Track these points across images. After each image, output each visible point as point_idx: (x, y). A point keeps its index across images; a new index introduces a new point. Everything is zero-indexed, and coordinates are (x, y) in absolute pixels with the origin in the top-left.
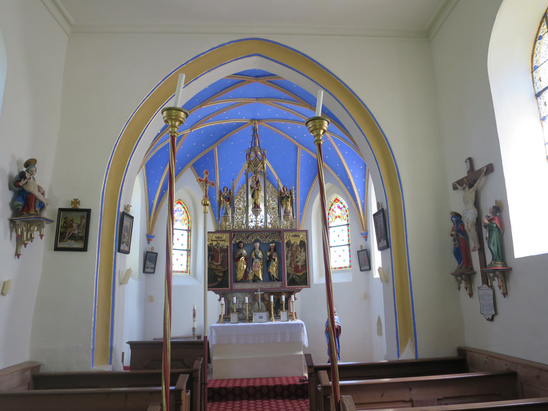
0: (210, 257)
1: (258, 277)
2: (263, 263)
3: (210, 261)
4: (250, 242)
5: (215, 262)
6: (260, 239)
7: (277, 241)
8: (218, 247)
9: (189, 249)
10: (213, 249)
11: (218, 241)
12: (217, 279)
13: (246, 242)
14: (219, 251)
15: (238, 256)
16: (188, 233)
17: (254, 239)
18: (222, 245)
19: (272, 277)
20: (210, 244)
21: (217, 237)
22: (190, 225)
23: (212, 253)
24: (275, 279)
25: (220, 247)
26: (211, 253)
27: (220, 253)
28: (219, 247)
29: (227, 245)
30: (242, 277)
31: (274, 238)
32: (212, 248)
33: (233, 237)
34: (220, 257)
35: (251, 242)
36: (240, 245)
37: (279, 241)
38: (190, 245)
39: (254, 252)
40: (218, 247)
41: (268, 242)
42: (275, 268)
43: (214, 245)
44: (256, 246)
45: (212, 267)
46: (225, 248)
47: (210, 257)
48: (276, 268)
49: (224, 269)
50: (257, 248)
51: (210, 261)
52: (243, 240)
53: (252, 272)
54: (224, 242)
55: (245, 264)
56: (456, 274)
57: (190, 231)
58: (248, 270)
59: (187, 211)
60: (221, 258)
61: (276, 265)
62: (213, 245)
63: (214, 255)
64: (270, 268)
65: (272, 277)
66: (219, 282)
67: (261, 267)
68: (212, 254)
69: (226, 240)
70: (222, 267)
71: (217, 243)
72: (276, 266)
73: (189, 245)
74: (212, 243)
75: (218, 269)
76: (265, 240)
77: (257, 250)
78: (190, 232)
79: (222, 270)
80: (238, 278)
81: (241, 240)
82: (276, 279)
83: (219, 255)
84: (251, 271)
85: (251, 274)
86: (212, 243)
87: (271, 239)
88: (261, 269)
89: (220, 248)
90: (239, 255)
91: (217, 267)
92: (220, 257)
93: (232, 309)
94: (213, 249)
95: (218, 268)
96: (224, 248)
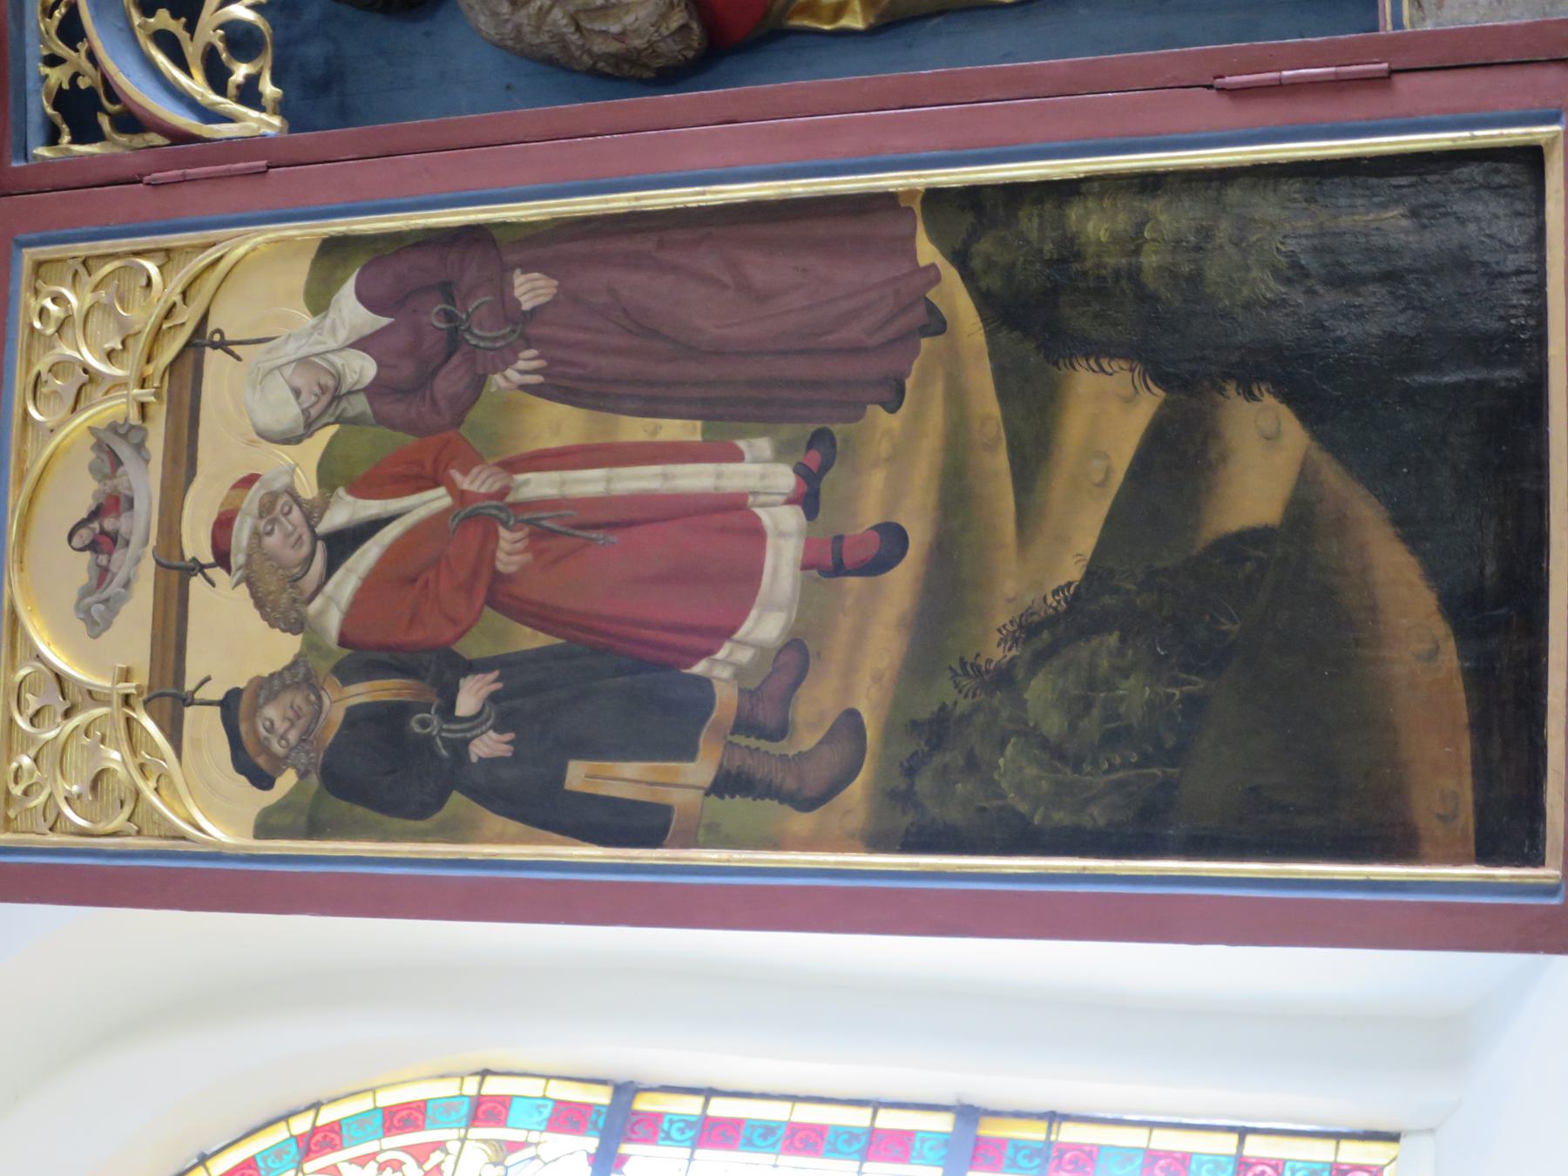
0: (579, 775)
3: (701, 770)
5: (726, 632)
8: (342, 544)
9: (943, 1123)
10: (362, 693)
11: (196, 543)
12: (1257, 537)
14: (436, 500)
16: (649, 1128)
18: (289, 413)
20: (263, 780)
21: (102, 575)
22: (533, 1087)
23: (469, 699)
25: (330, 474)
26: (488, 745)
27: (478, 482)
28: (344, 512)
29: (299, 272)
32: (356, 718)
33: (132, 121)
34: (589, 482)
38: (877, 1105)
40: (342, 544)
43: (282, 648)
45: (870, 706)
46: (369, 321)
47: (579, 775)
49: (936, 324)
51: (701, 770)
54: (214, 360)
57: (625, 1090)
59: (301, 1125)
60: (634, 429)
62: (267, 687)
63: (531, 639)
66: (1332, 475)
68: (501, 712)
69: (188, 317)
70: (894, 398)
71: (222, 558)
73: (859, 1118)
74: (230, 705)
75: (944, 550)
78: (644, 1104)
79: (957, 397)
83: (538, 485)
86: (230, 705)
89: (363, 488)
91: (893, 540)
92: (589, 482)
94: (362, 693)
95: (919, 536)
96: (362, 368)
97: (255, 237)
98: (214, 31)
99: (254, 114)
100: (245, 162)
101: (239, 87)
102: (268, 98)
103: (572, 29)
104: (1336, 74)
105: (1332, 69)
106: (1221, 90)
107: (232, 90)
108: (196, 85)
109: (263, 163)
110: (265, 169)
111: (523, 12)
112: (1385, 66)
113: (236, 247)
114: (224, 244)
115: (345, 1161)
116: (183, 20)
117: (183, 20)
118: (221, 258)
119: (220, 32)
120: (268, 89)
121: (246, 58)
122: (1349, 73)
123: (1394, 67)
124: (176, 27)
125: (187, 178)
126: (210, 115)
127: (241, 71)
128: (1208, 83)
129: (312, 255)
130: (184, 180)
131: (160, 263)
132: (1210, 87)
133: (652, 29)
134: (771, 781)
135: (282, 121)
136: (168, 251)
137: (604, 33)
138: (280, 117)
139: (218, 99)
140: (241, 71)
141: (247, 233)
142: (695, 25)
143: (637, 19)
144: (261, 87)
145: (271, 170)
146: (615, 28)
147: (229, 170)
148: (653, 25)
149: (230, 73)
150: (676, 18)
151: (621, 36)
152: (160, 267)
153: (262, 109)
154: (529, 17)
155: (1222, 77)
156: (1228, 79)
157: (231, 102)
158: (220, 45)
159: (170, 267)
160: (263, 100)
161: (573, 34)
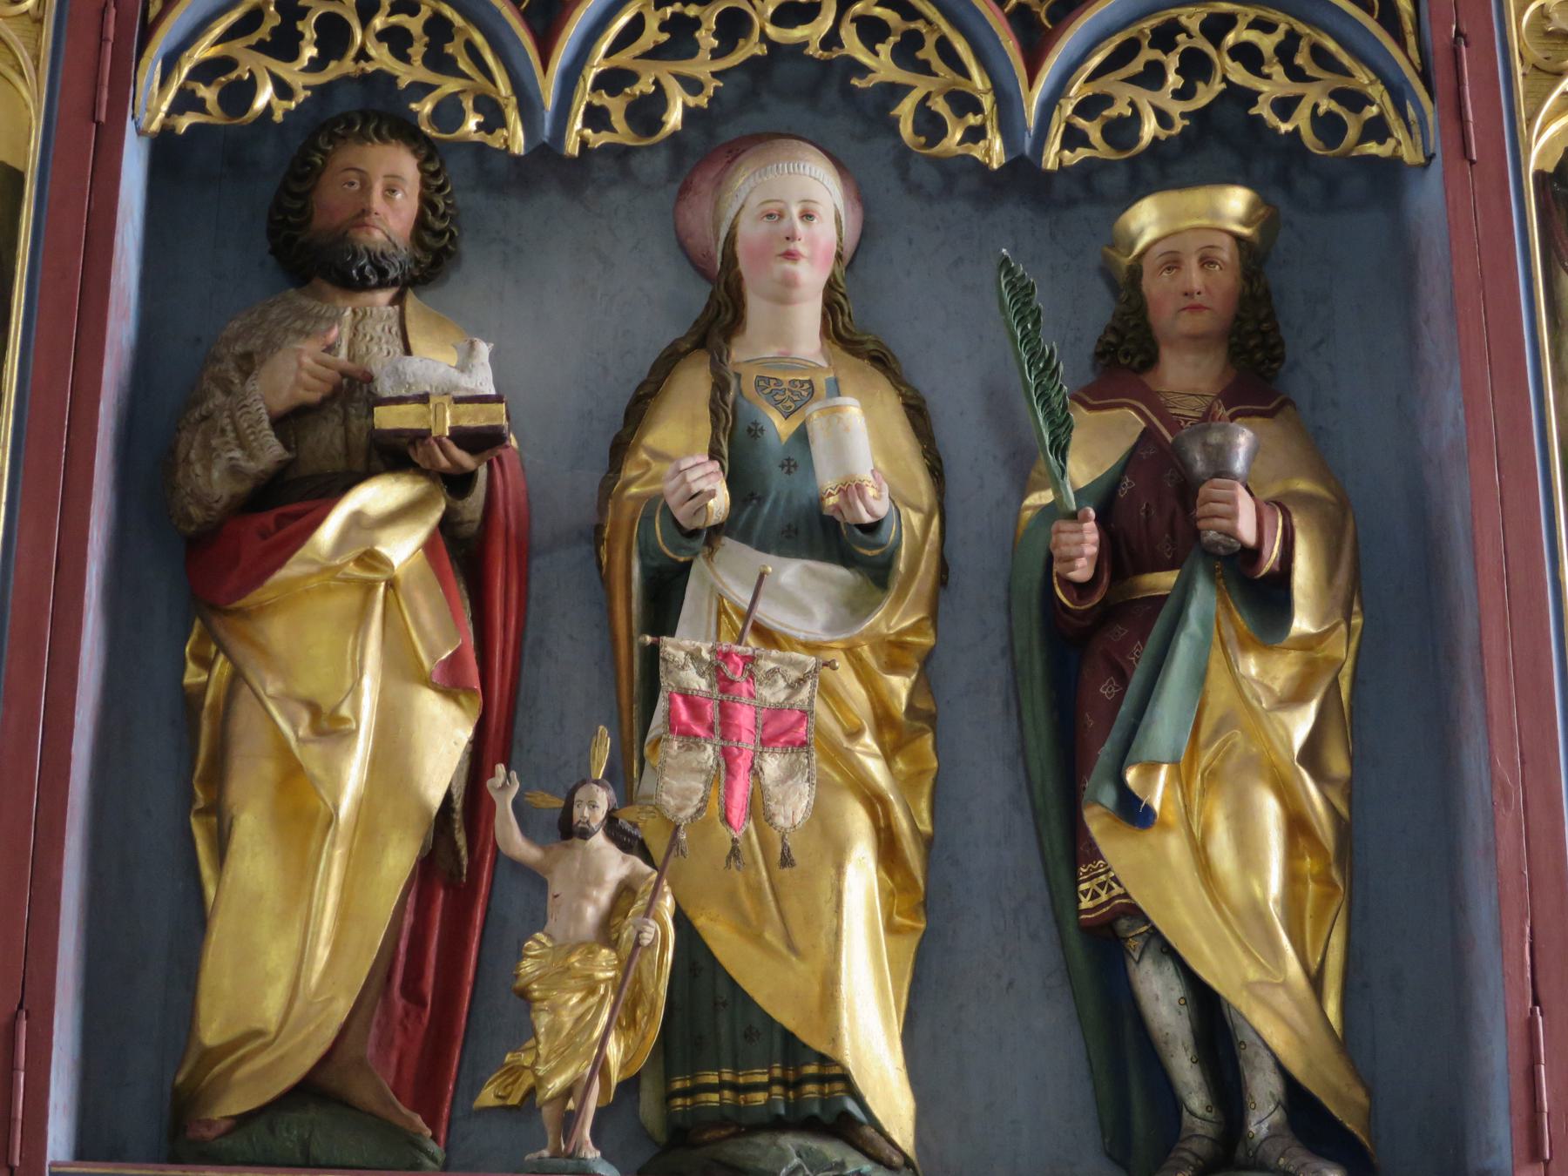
1: (791, 1048)
2: (928, 671)
4: (597, 118)
6: (882, 65)
7: (1329, 127)
13: (494, 118)
15: (272, 450)
17: (702, 67)
19: (1186, 1070)
24: (1264, 1117)
30: (342, 1008)
31: (1248, 56)
35: (622, 132)
36: (332, 195)
37: (1377, 130)
39: (693, 384)
41: (1073, 138)
42: (1270, 810)
44: (751, 231)
48: (1297, 826)
50: (785, 290)
52: (439, 62)
53: (626, 890)
55: (450, 684)
56: (266, 1046)
58: (514, 840)
61: (1301, 724)
64: (1134, 812)
65: (1186, 1070)
67: (876, 768)
72: (1312, 754)
76: (1007, 103)
77: (781, 333)
80: (212, 1032)
81: (382, 57)
82: (1296, 1097)
84: (615, 865)
85: (607, 932)
87: (1153, 77)
88: (888, 850)
90: (290, 422)
93: (687, 789)
97: (34, 108)
98: (250, 71)
99: (165, 107)
100: (108, 101)
101: (193, 92)
102: (177, 121)
103: (204, 413)
104: (15, 1119)
105: (20, 1116)
106: (16, 1017)
107: (192, 85)
108: (203, 50)
109: (103, 118)
110: (96, 119)
111: (232, 365)
112: (17, 1163)
113: (28, 88)
114: (34, 78)
115: (1184, 309)
116: (268, 39)
117: (268, 39)
118: (22, 74)
119: (246, 76)
120: (184, 123)
121: (222, 99)
122: (15, 1131)
123: (16, 1171)
124: (263, 32)
125: (103, 43)
126: (170, 62)
127: (209, 94)
128: (24, 1005)
129: (10, 162)
130: (102, 39)
131: (31, 12)
132: (20, 1006)
133: (189, 490)
134: (774, 815)
135: (155, 133)
136: (39, 21)
137: (191, 446)
138: (158, 131)
139: (185, 71)
140: (209, 94)
141: (39, 101)
142: (193, 528)
143: (197, 475)
144: (189, 113)
145: (95, 125)
146: (193, 456)
147: (102, 84)
148: (192, 490)
149: (208, 84)
150: (198, 512)
151: (187, 461)
152: (27, 12)
153: (168, 114)
154: (227, 371)
155: (27, 1018)
156: (25, 1022)
157: (180, 82)
158: (233, 76)
159: (26, 23)
160: (176, 116)
161: (200, 414)
